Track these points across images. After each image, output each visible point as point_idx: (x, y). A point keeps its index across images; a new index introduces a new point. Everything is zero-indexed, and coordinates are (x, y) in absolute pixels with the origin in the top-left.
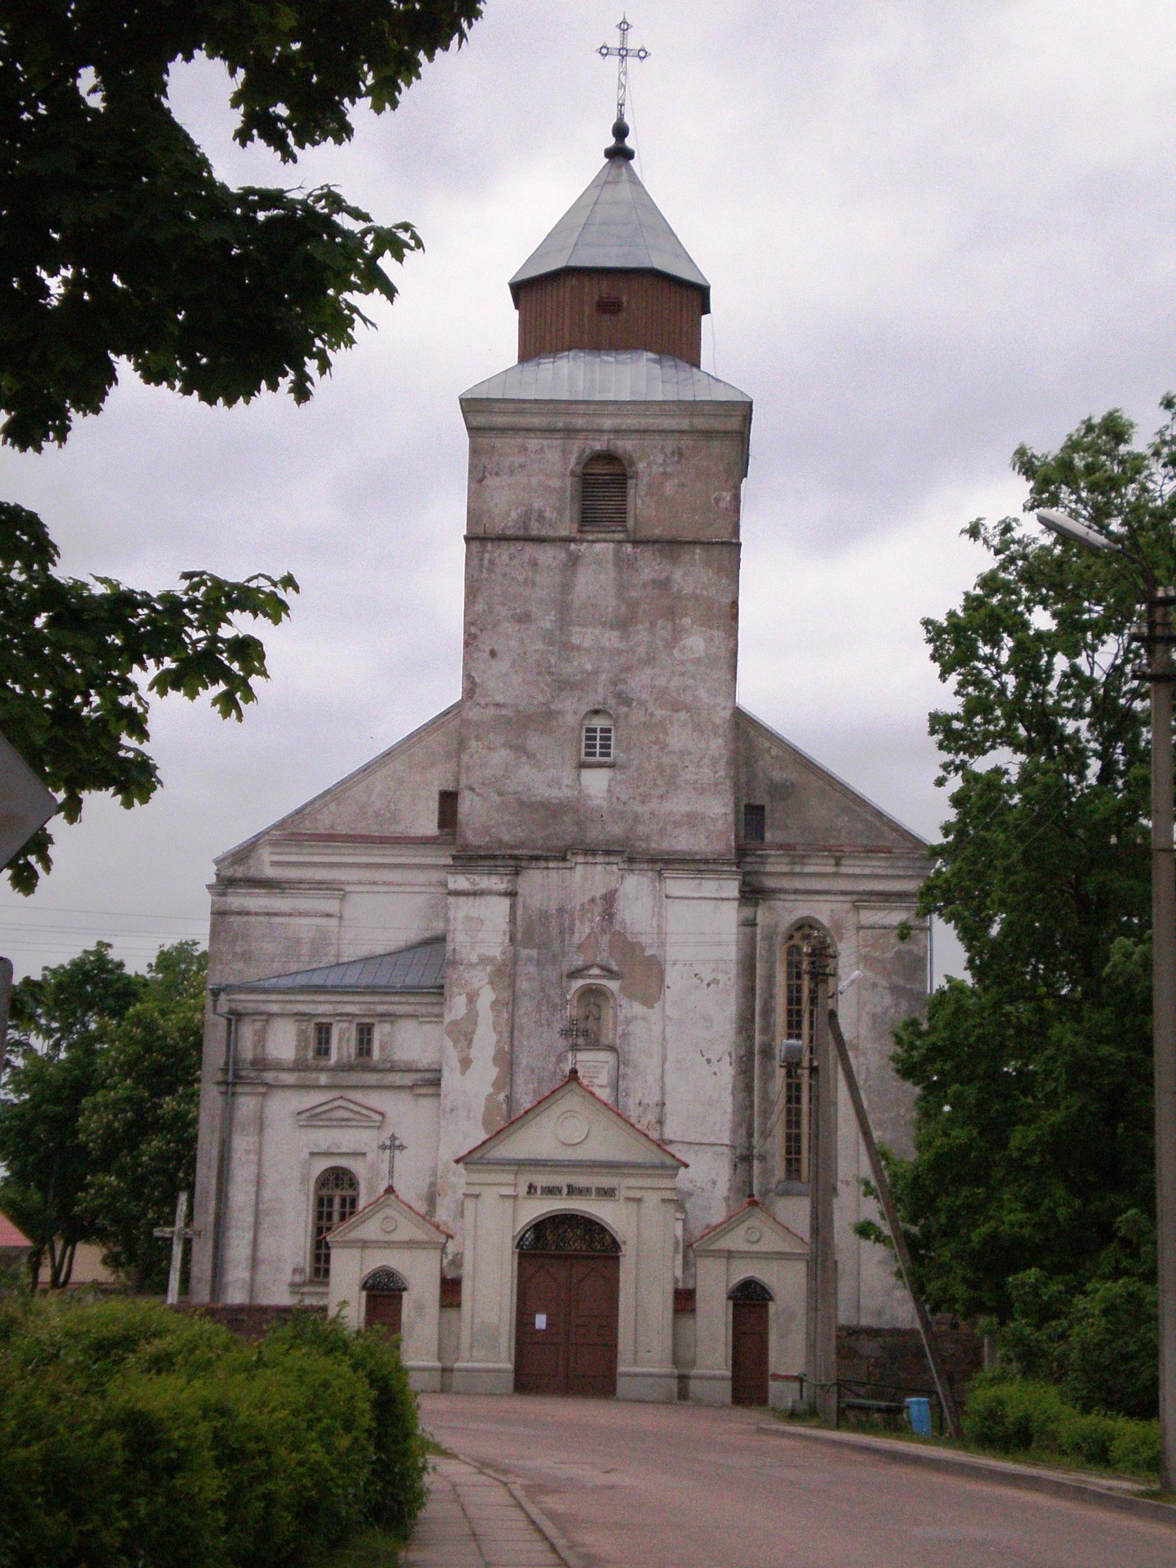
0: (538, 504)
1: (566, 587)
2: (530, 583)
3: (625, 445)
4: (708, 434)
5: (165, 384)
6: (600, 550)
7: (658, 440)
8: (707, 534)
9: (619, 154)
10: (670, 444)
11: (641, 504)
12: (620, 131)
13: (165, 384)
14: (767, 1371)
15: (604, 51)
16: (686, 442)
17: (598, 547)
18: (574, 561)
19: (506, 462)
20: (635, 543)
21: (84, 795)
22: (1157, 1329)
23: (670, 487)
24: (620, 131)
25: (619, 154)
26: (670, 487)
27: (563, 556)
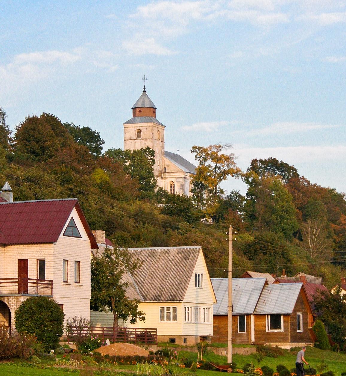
0: (132, 136)
1: (135, 145)
2: (131, 145)
3: (140, 128)
4: (149, 126)
5: (30, 118)
6: (138, 140)
7: (144, 127)
8: (150, 138)
9: (144, 91)
10: (146, 127)
11: (143, 135)
12: (144, 89)
13: (30, 118)
14: (272, 342)
15: (147, 79)
16: (147, 127)
17: (138, 140)
18: (135, 142)
19: (128, 131)
20: (142, 139)
21: (275, 280)
22: (329, 339)
23: (145, 132)
24: (144, 89)
25: (144, 91)
26: (145, 132)
27: (134, 141)
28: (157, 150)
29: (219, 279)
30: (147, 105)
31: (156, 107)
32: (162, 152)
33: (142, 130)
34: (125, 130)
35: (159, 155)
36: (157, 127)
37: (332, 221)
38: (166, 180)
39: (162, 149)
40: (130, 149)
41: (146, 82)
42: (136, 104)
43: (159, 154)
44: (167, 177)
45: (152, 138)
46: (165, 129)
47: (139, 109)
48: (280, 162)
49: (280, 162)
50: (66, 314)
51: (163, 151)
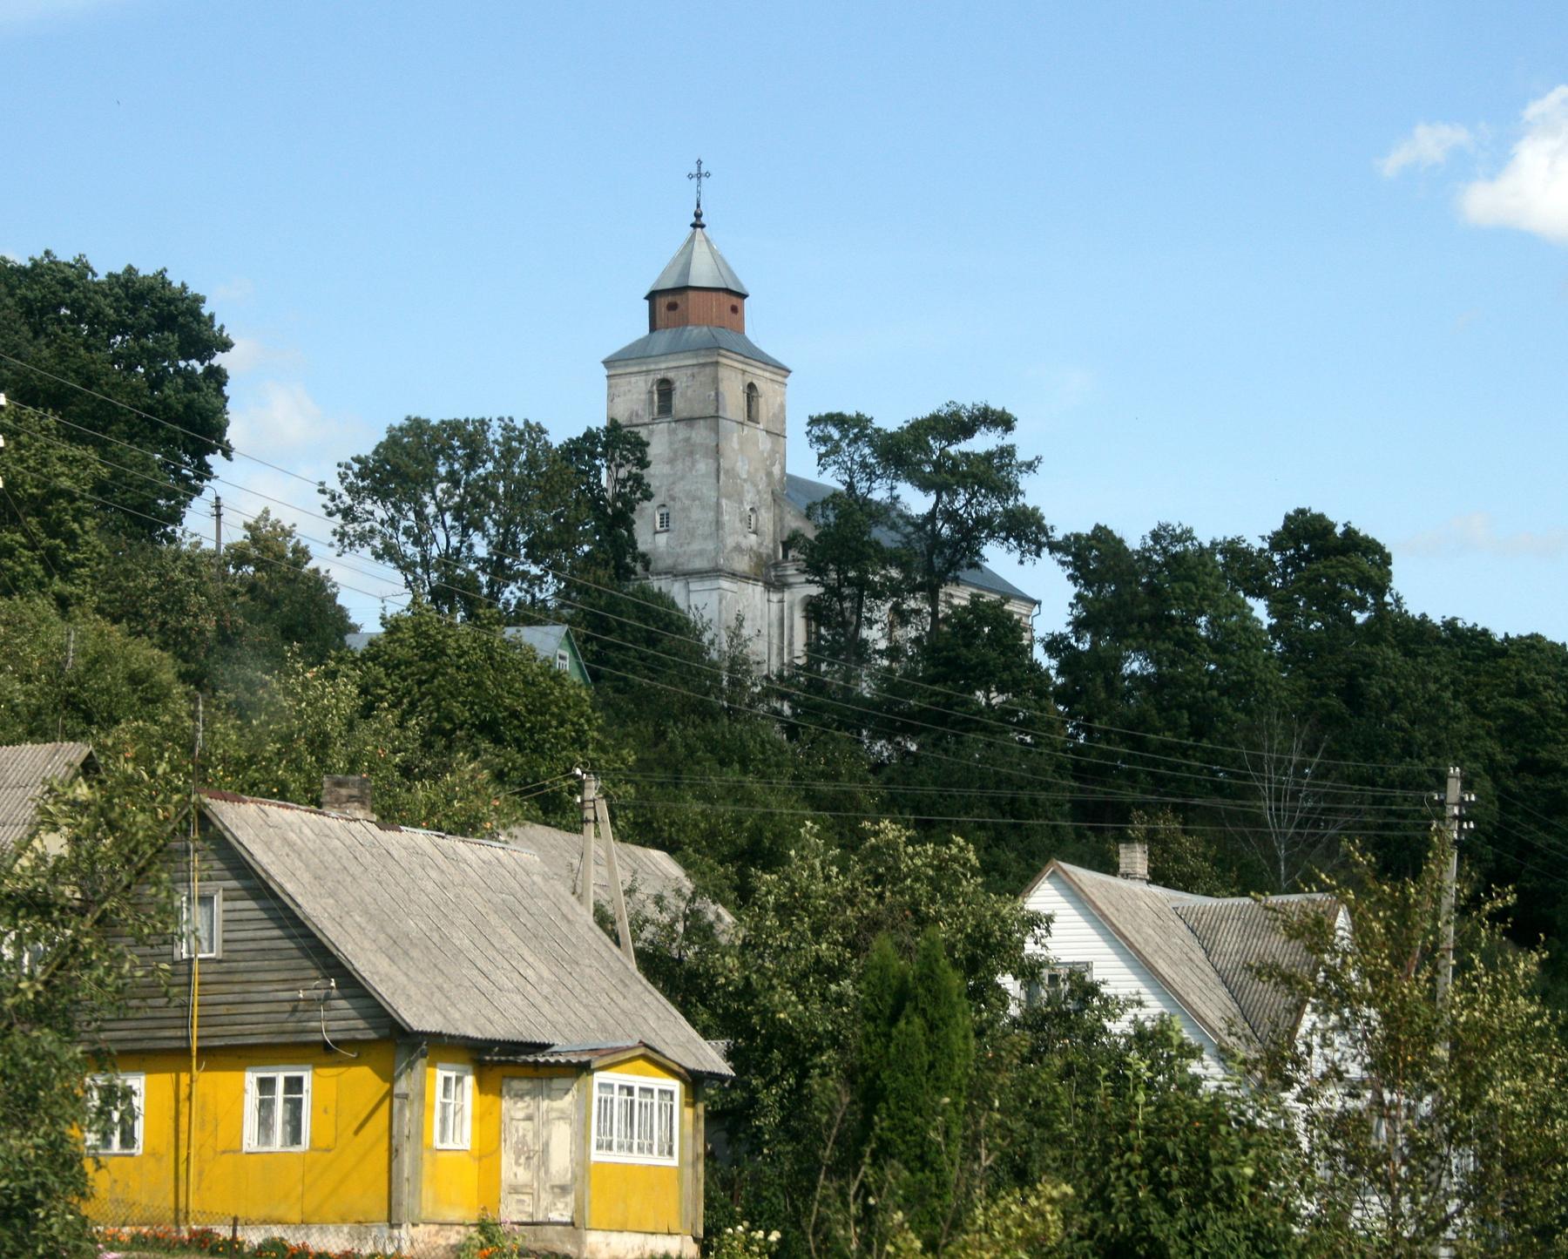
3: (670, 375)
4: (704, 365)
7: (684, 371)
10: (689, 372)
11: (678, 403)
12: (698, 216)
23: (689, 392)
24: (698, 216)
26: (689, 392)
28: (739, 464)
29: (696, 1219)
30: (702, 274)
31: (748, 287)
32: (769, 474)
33: (677, 384)
34: (610, 387)
35: (753, 490)
36: (744, 372)
37: (898, 1095)
38: (787, 595)
39: (773, 464)
40: (339, 465)
41: (703, 189)
42: (658, 281)
43: (756, 486)
44: (791, 580)
45: (712, 413)
46: (787, 381)
47: (670, 299)
48: (1339, 530)
49: (1339, 530)
50: (1104, 983)
51: (776, 470)
